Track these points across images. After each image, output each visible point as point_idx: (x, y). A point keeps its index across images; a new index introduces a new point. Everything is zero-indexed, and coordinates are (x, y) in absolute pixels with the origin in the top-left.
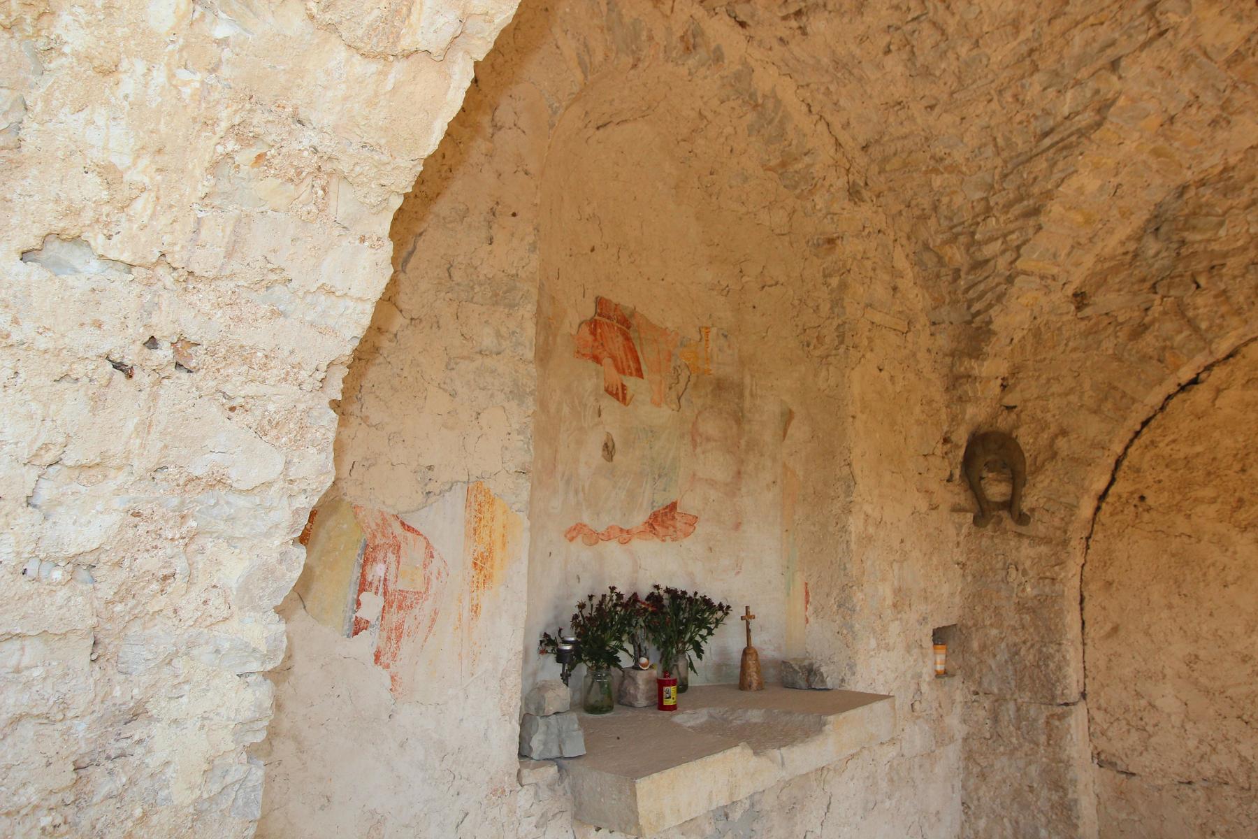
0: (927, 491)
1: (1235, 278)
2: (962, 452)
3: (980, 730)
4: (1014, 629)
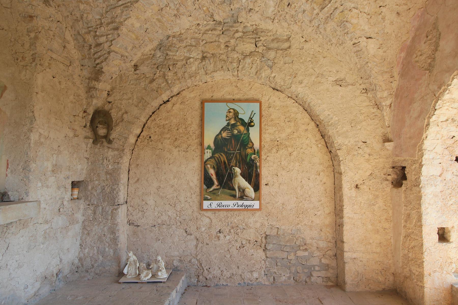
0: (73, 129)
1: (179, 68)
2: (90, 117)
3: (89, 218)
4: (104, 181)
